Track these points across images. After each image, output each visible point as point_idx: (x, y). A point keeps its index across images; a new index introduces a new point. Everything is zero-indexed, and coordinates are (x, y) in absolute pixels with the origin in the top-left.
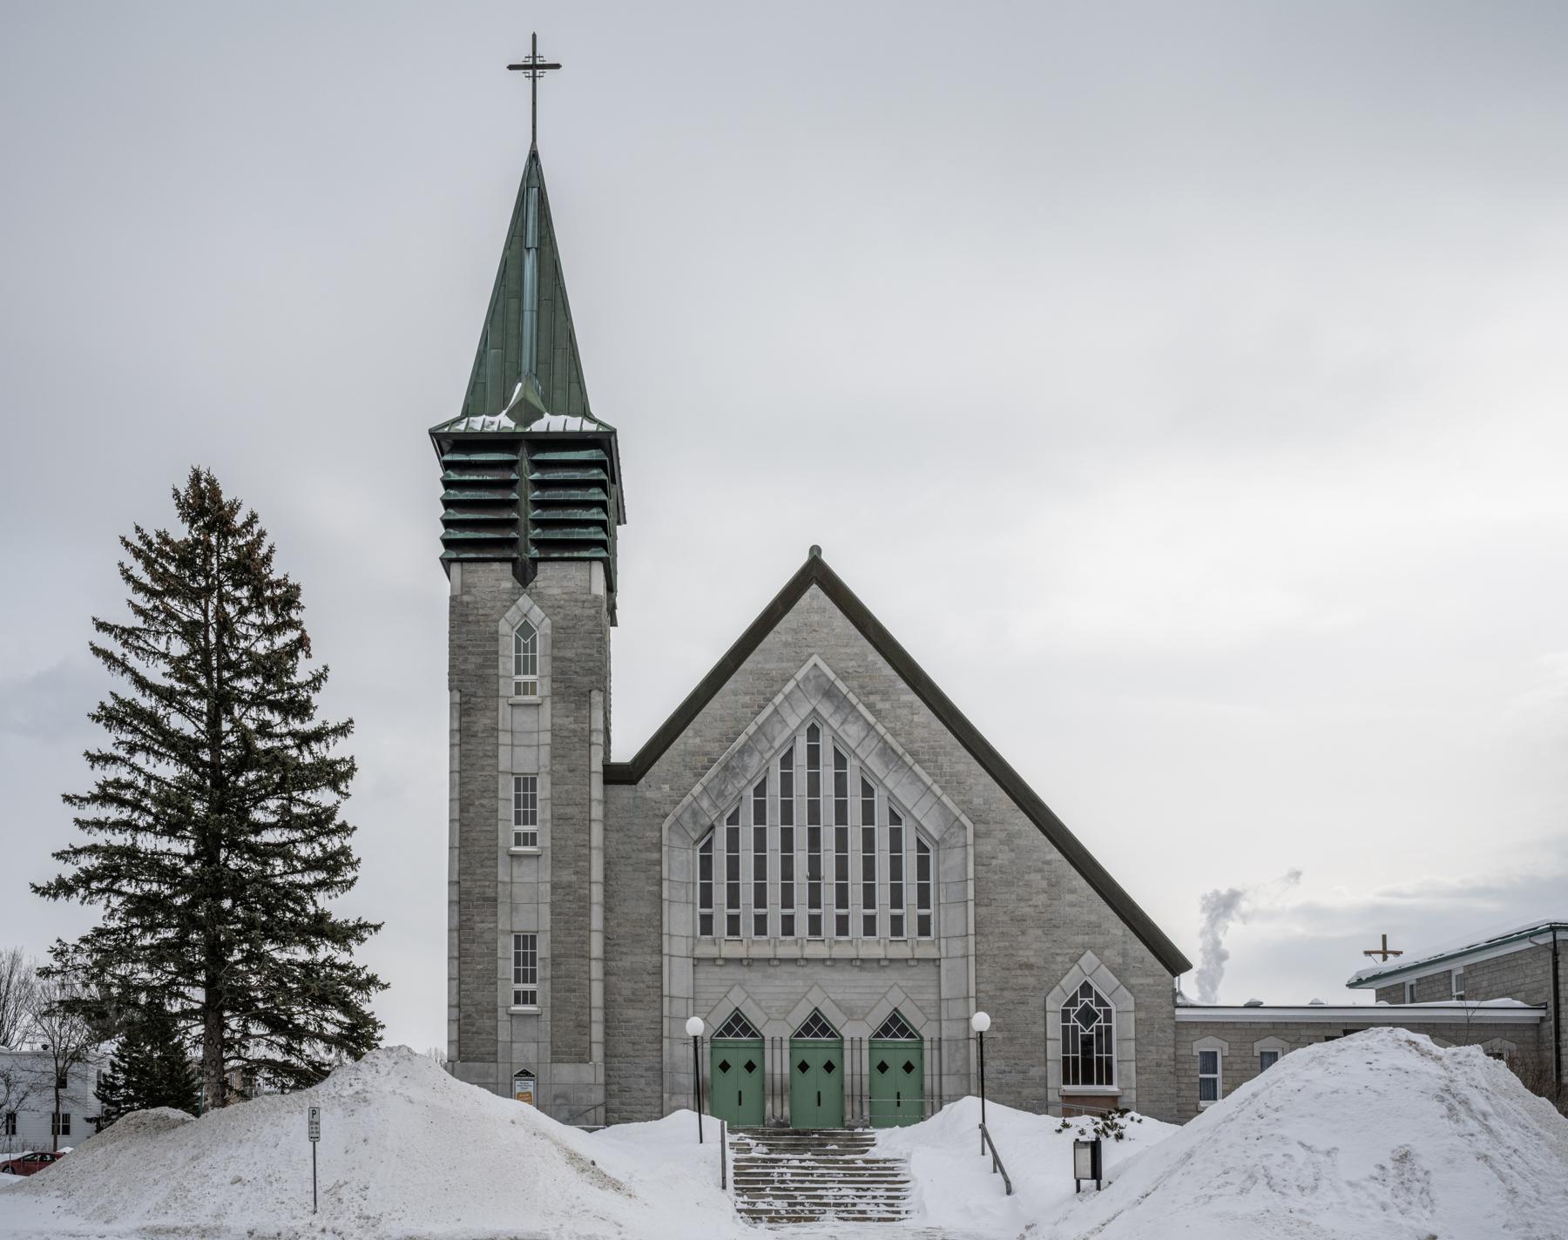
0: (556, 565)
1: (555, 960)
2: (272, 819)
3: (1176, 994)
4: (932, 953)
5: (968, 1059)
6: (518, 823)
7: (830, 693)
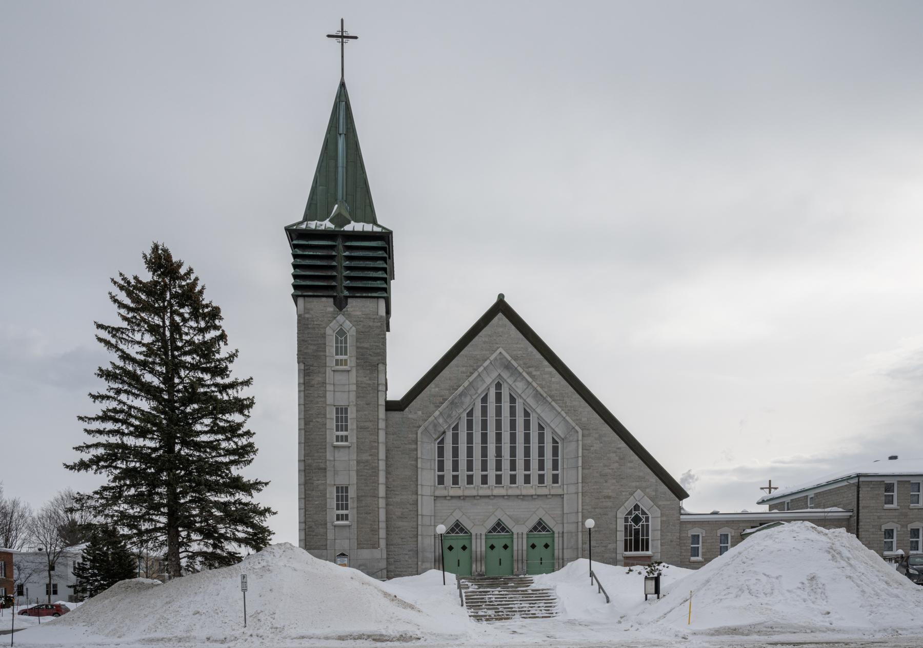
0: (359, 300)
1: (359, 499)
2: (206, 429)
3: (681, 508)
4: (560, 492)
5: (577, 541)
6: (337, 430)
7: (508, 366)
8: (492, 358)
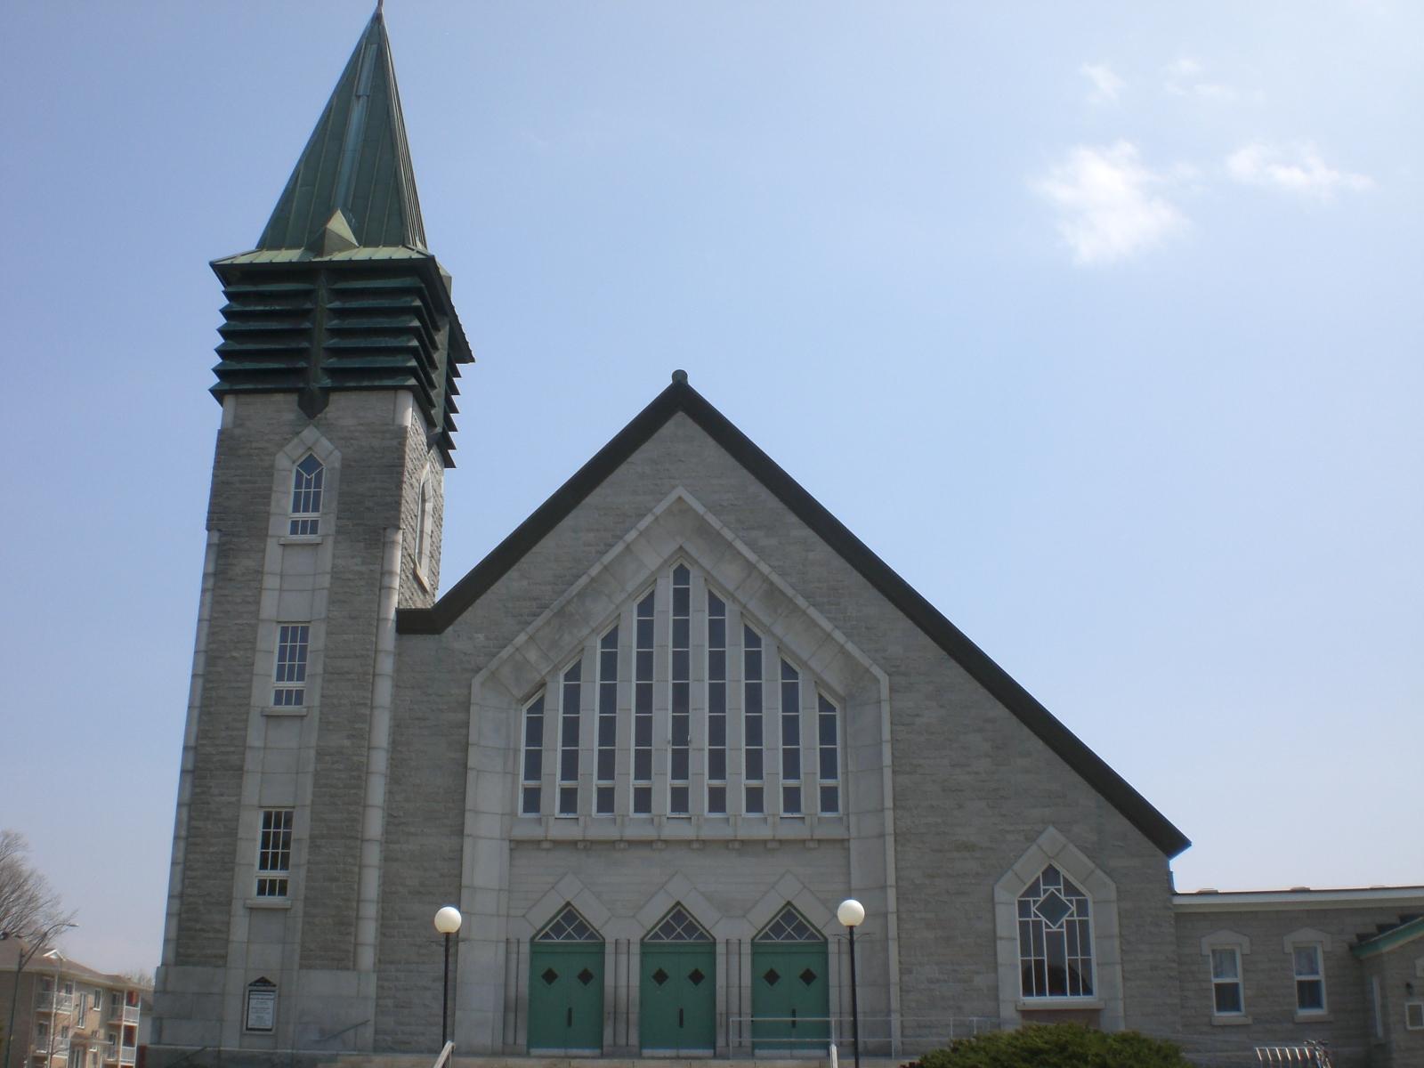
0: (353, 396)
4: (837, 832)
8: (659, 510)
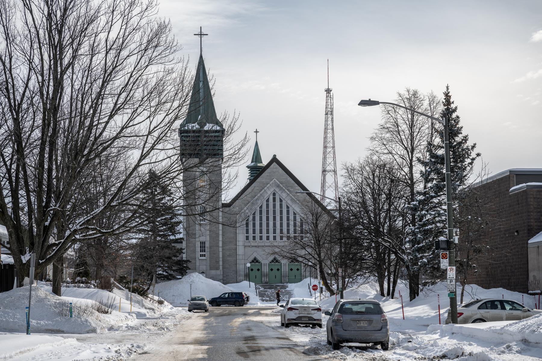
1: (210, 247)
7: (278, 186)
